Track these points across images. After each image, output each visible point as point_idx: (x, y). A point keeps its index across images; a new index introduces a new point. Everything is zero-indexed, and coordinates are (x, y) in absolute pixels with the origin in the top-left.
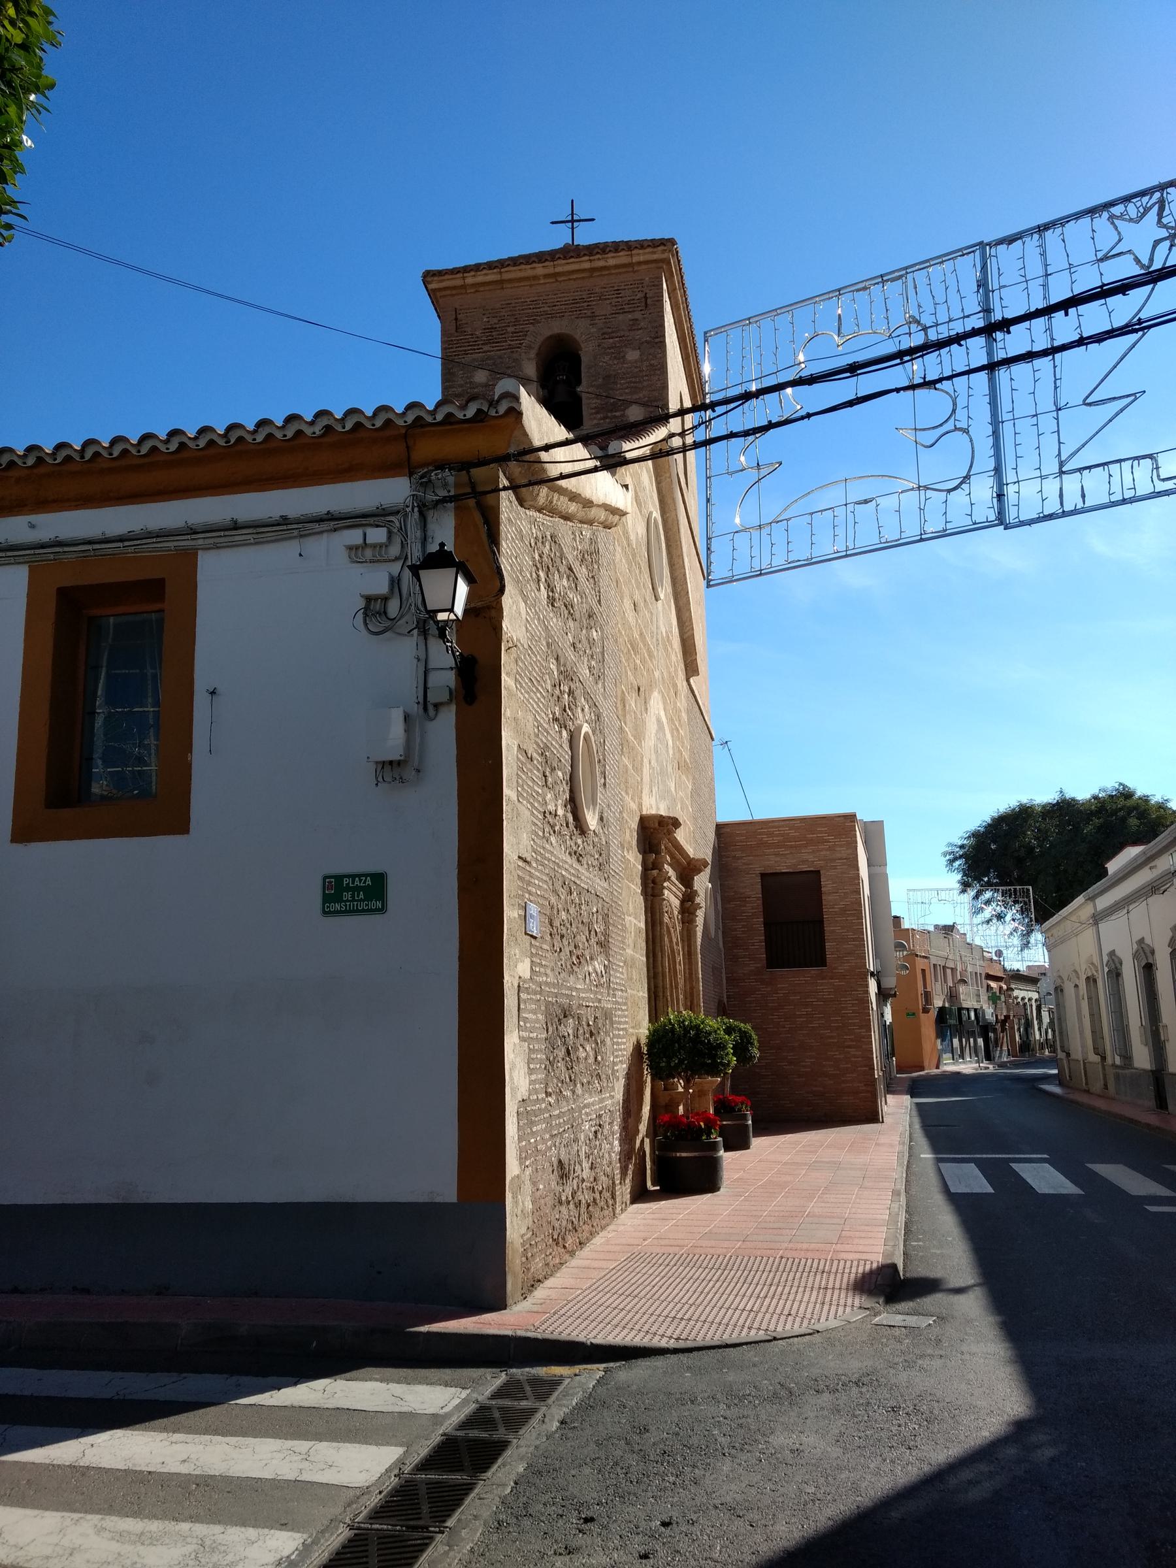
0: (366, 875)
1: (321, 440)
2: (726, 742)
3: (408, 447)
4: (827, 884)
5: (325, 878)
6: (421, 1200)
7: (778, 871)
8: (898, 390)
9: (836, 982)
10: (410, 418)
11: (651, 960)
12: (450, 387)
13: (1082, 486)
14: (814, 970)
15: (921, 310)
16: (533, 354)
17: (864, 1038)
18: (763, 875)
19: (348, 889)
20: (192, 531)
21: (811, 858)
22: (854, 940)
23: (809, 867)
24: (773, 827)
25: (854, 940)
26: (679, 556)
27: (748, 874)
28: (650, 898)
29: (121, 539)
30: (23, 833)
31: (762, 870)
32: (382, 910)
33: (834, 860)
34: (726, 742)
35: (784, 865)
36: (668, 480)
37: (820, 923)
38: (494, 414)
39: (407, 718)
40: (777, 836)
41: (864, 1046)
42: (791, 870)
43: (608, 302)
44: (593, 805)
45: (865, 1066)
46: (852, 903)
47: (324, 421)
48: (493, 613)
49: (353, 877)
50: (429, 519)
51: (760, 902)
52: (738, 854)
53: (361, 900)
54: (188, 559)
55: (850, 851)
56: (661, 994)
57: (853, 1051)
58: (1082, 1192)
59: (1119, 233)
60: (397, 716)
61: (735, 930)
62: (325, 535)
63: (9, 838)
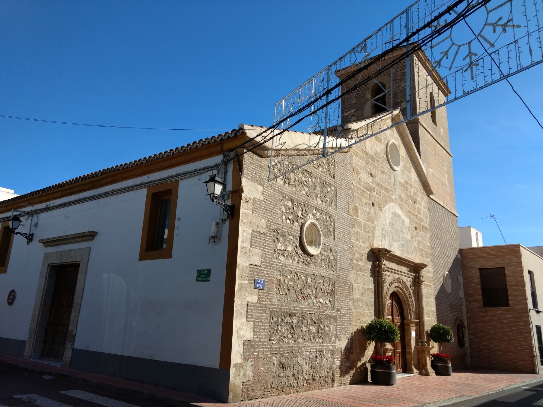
0: (206, 270)
1: (202, 147)
2: (493, 216)
3: (222, 147)
4: (508, 273)
5: (198, 271)
6: (211, 367)
7: (486, 267)
8: (307, 116)
9: (514, 314)
10: (220, 138)
11: (377, 300)
12: (344, 106)
13: (341, 142)
14: (504, 308)
15: (538, 40)
16: (370, 90)
17: (528, 338)
18: (480, 269)
19: (202, 274)
20: (178, 175)
21: (500, 262)
22: (522, 296)
23: (500, 266)
24: (484, 250)
25: (522, 296)
26: (414, 153)
27: (473, 268)
28: (377, 278)
29: (164, 179)
30: (141, 258)
31: (479, 267)
32: (209, 280)
33: (511, 263)
34: (493, 216)
35: (489, 264)
36: (403, 128)
37: (505, 289)
38: (239, 134)
39: (217, 224)
40: (485, 253)
41: (528, 341)
42: (492, 267)
43: (395, 68)
44: (319, 246)
45: (529, 349)
46: (520, 281)
47: (201, 142)
48: (240, 192)
49: (203, 270)
50: (228, 166)
51: (479, 280)
52: (469, 261)
53: (205, 277)
54: (177, 182)
55: (518, 260)
56: (381, 312)
57: (523, 343)
58: (535, 404)
59: (356, 57)
60: (214, 223)
61: (469, 290)
62: (205, 173)
63: (138, 260)
